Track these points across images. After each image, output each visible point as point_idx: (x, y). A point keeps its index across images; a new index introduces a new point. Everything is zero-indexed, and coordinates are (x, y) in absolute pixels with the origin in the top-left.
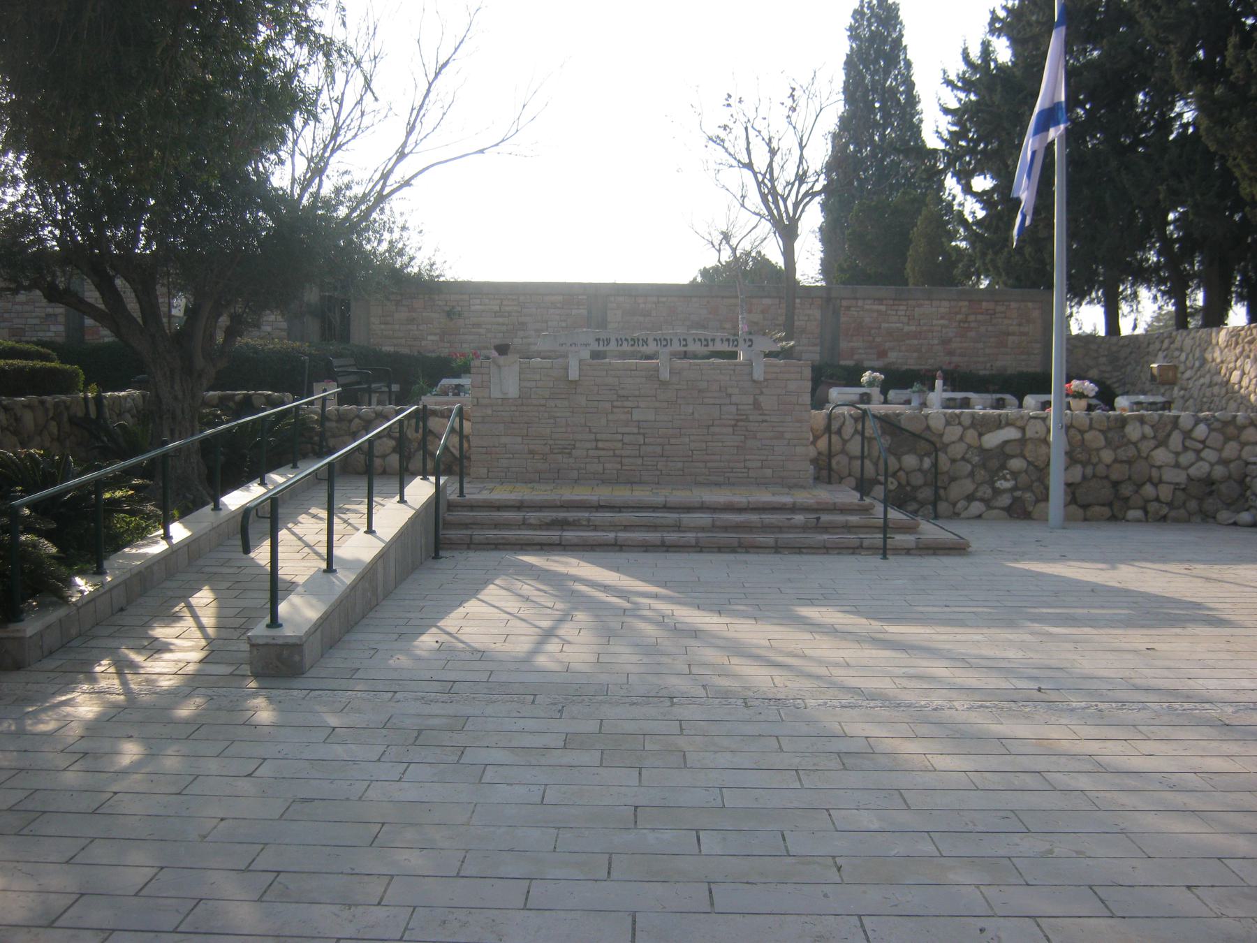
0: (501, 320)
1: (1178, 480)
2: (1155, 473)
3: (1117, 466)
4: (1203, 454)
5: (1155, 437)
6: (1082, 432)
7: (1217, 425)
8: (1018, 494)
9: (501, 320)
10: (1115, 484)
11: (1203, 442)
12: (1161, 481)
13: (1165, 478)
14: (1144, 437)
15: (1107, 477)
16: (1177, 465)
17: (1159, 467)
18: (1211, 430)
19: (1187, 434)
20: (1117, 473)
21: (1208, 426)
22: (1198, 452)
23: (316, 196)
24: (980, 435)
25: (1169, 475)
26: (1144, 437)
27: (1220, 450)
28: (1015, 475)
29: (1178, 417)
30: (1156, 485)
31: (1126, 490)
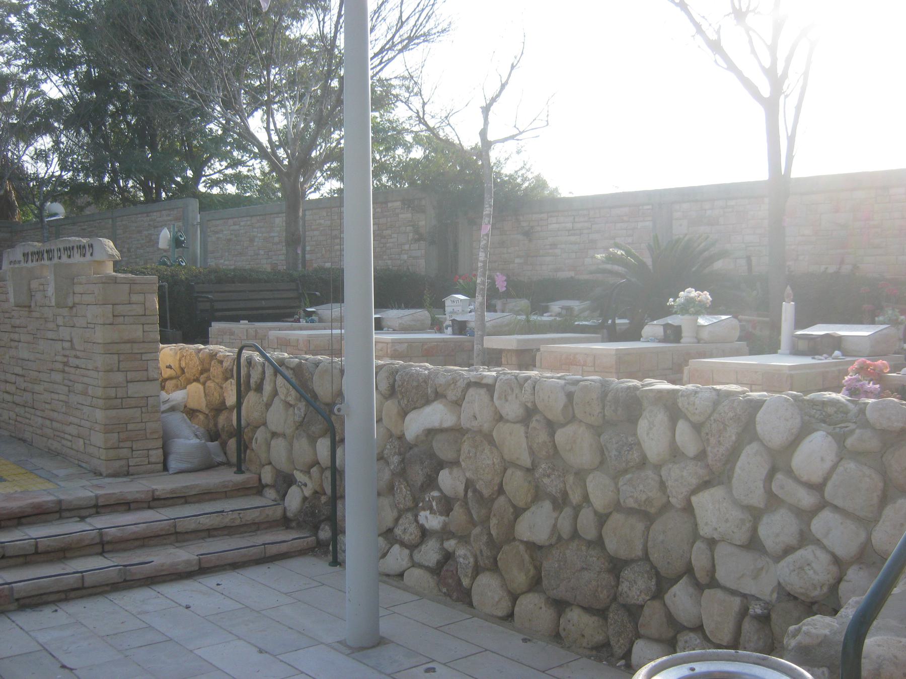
0: (573, 238)
1: (749, 587)
2: (699, 560)
3: (617, 519)
4: (818, 525)
5: (701, 456)
6: (551, 427)
7: (856, 439)
8: (450, 544)
9: (573, 238)
10: (616, 566)
11: (818, 488)
12: (713, 583)
13: (721, 575)
14: (675, 454)
15: (599, 543)
16: (753, 544)
17: (712, 543)
18: (843, 453)
19: (779, 461)
20: (622, 537)
21: (840, 439)
22: (806, 515)
23: (277, 131)
24: (404, 414)
25: (732, 567)
26: (675, 454)
27: (868, 522)
28: (447, 505)
29: (757, 405)
30: (700, 587)
31: (635, 586)
